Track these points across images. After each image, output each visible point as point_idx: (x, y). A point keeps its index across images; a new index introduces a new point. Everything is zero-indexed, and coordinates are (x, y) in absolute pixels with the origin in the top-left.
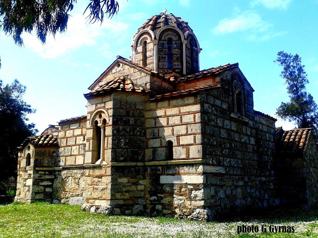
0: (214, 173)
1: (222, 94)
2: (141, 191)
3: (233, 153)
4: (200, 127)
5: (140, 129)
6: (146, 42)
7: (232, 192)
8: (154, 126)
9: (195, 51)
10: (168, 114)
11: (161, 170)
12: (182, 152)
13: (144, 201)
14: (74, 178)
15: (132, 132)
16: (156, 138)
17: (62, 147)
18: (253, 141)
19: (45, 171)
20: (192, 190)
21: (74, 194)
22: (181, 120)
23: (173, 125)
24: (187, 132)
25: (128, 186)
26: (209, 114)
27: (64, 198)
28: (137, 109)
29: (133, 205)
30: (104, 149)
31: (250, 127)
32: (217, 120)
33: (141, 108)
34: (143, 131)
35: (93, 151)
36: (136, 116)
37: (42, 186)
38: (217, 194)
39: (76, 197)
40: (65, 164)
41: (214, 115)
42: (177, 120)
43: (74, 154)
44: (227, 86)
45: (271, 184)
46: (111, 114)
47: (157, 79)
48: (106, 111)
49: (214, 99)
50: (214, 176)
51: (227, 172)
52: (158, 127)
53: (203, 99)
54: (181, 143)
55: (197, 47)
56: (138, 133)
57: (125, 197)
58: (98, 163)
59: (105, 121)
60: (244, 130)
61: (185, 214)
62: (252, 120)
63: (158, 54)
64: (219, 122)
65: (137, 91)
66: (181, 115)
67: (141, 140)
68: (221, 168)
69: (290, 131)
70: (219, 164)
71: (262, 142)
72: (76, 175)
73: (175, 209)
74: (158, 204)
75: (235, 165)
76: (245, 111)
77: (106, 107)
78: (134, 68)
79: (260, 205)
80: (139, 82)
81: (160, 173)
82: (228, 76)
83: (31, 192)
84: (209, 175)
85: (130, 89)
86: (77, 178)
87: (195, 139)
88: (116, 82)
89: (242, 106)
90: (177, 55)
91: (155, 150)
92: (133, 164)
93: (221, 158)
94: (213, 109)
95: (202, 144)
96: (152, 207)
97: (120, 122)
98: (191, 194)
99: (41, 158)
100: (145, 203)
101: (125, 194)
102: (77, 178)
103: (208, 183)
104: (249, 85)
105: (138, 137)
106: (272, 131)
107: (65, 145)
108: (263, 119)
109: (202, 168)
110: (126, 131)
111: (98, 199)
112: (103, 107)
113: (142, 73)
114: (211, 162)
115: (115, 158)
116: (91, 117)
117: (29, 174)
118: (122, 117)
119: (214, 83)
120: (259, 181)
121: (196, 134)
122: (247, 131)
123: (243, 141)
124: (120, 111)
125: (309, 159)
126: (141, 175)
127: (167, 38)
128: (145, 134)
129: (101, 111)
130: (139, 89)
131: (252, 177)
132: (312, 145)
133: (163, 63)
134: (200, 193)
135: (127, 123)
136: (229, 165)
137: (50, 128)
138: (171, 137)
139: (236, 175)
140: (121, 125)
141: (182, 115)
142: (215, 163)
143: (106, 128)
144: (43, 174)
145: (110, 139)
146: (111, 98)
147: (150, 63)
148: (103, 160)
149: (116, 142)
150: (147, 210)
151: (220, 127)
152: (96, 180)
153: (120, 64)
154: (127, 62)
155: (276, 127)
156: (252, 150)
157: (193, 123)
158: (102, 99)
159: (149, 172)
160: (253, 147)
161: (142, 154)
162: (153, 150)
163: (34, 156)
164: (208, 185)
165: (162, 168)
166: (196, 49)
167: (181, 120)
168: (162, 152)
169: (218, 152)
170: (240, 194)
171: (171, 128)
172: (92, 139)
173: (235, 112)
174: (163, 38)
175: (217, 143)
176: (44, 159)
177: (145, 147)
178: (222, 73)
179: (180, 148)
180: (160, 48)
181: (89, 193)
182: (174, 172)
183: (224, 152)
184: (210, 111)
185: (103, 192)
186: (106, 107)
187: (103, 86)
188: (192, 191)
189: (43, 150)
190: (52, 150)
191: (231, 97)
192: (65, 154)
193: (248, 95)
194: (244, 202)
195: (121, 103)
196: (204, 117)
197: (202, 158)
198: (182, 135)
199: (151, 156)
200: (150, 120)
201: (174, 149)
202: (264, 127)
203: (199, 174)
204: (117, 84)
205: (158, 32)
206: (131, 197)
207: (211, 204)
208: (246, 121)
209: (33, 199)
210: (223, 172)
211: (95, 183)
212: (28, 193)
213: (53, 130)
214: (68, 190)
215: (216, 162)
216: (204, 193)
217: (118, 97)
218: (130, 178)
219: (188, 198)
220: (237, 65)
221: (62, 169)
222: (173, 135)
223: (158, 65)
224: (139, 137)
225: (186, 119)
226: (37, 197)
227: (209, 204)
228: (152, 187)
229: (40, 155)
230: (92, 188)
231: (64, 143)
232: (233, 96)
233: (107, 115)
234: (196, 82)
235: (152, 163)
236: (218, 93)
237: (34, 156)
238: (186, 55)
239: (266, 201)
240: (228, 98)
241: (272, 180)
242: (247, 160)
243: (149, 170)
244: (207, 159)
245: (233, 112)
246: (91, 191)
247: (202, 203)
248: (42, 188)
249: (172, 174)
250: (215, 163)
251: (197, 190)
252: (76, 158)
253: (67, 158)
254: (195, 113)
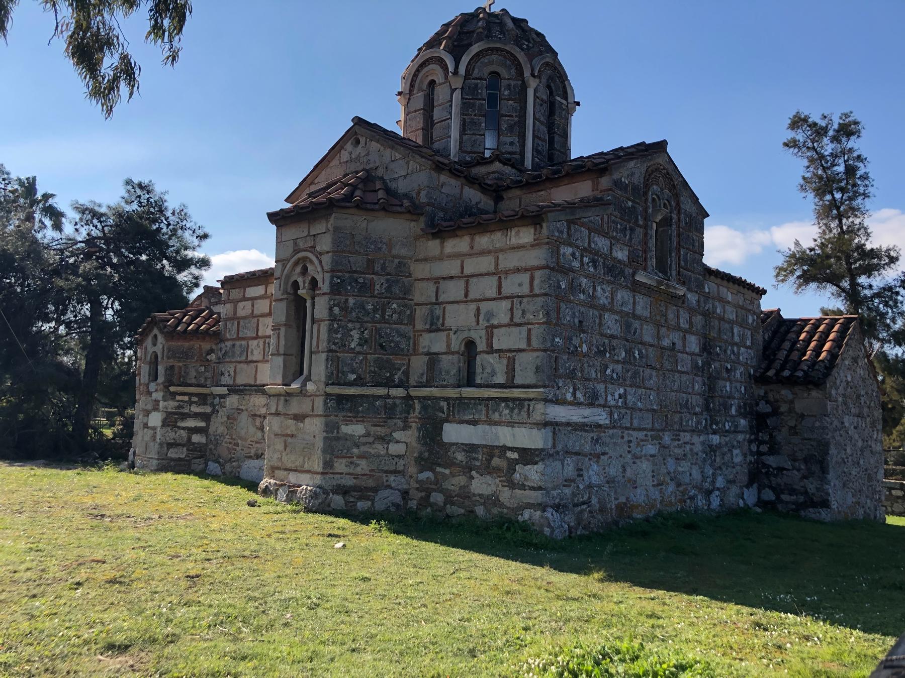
0: (576, 424)
1: (614, 222)
2: (396, 456)
3: (636, 374)
7: (624, 470)
8: (434, 301)
11: (445, 408)
12: (497, 370)
13: (403, 480)
15: (380, 312)
16: (438, 330)
18: (693, 343)
19: (191, 395)
25: (365, 444)
28: (394, 257)
29: (375, 490)
30: (311, 353)
32: (594, 290)
33: (403, 252)
34: (408, 312)
35: (287, 355)
36: (389, 274)
37: (184, 428)
42: (487, 287)
43: (254, 359)
45: (735, 452)
47: (449, 179)
48: (317, 257)
50: (575, 430)
51: (615, 422)
52: (442, 303)
53: (557, 234)
56: (395, 316)
57: (359, 470)
59: (314, 283)
60: (671, 316)
63: (462, 114)
64: (603, 295)
66: (499, 274)
70: (592, 401)
71: (720, 347)
74: (434, 490)
75: (639, 404)
77: (318, 248)
81: (443, 416)
82: (637, 176)
86: (260, 416)
89: (670, 254)
90: (511, 116)
91: (433, 358)
93: (601, 387)
96: (422, 497)
97: (349, 288)
99: (181, 364)
100: (405, 487)
101: (358, 462)
103: (559, 447)
106: (750, 321)
110: (364, 308)
112: (310, 247)
114: (569, 397)
118: (355, 275)
119: (596, 193)
120: (703, 443)
123: (666, 344)
127: (486, 71)
128: (411, 320)
129: (307, 257)
133: (474, 138)
135: (365, 289)
136: (620, 404)
140: (353, 295)
142: (582, 400)
144: (186, 402)
145: (324, 327)
148: (308, 378)
149: (339, 336)
150: (409, 502)
151: (603, 308)
156: (689, 366)
159: (417, 411)
160: (692, 360)
161: (402, 369)
162: (429, 358)
164: (558, 453)
165: (448, 404)
166: (564, 102)
172: (285, 325)
175: (589, 348)
176: (187, 368)
177: (411, 351)
179: (491, 359)
180: (466, 99)
182: (477, 417)
183: (608, 371)
184: (576, 264)
191: (639, 231)
194: (655, 494)
195: (353, 238)
196: (558, 282)
198: (499, 326)
199: (422, 374)
200: (424, 284)
207: (561, 499)
208: (678, 292)
209: (163, 459)
210: (601, 422)
218: (372, 425)
220: (661, 146)
223: (461, 143)
225: (511, 286)
228: (424, 449)
229: (179, 357)
233: (319, 269)
234: (550, 189)
235: (425, 392)
236: (602, 219)
238: (535, 118)
241: (739, 442)
242: (672, 391)
243: (418, 407)
248: (183, 433)
249: (473, 421)
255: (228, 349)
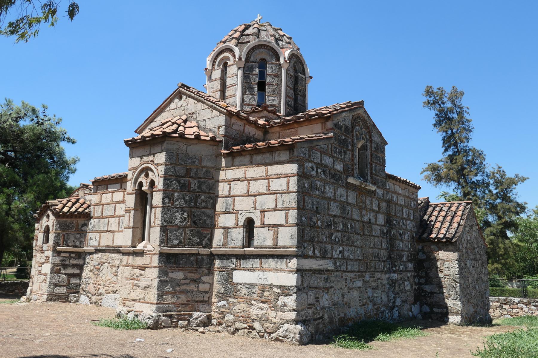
0: (315, 270)
3: (349, 238)
4: (296, 199)
5: (206, 198)
6: (227, 63)
9: (301, 80)
10: (249, 176)
14: (110, 266)
17: (95, 219)
18: (381, 219)
20: (279, 295)
21: (110, 289)
22: (268, 186)
23: (255, 193)
24: (276, 205)
25: (183, 285)
26: (311, 179)
27: (96, 294)
30: (150, 227)
31: (379, 199)
32: (325, 188)
33: (209, 164)
34: (211, 201)
36: (200, 178)
38: (318, 301)
39: (112, 294)
40: (99, 244)
41: (321, 180)
44: (344, 135)
46: (162, 173)
47: (237, 121)
49: (321, 155)
53: (302, 155)
54: (266, 223)
55: (304, 74)
58: (140, 247)
60: (368, 203)
61: (267, 330)
62: (382, 188)
64: (329, 191)
65: (202, 138)
67: (208, 214)
68: (326, 261)
69: (440, 204)
70: (324, 255)
72: (113, 261)
73: (253, 322)
76: (372, 173)
77: (156, 162)
78: (203, 102)
79: (387, 315)
80: (209, 125)
82: (347, 121)
83: (48, 282)
84: (306, 272)
85: (193, 135)
86: (115, 266)
87: (287, 216)
88: (174, 123)
89: (367, 166)
92: (194, 250)
93: (329, 247)
94: (319, 170)
95: (297, 225)
98: (277, 302)
101: (179, 296)
102: (115, 266)
103: (305, 286)
104: (380, 135)
105: (203, 210)
106: (412, 205)
107: (100, 215)
108: (398, 187)
109: (296, 262)
111: (139, 301)
113: (214, 111)
114: (311, 253)
115: (164, 242)
116: (133, 175)
117: (47, 257)
121: (289, 210)
122: (372, 204)
124: (176, 168)
125: (466, 248)
126: (205, 268)
130: (208, 136)
131: (376, 274)
132: (471, 227)
134: (291, 301)
136: (340, 257)
137: (82, 189)
138: (252, 211)
139: (351, 272)
141: (270, 179)
142: (318, 255)
143: (154, 193)
145: (159, 211)
146: (163, 148)
147: (231, 96)
151: (330, 199)
152: (137, 272)
153: (183, 96)
154: (193, 93)
155: (419, 198)
156: (379, 232)
157: (286, 193)
158: (150, 149)
163: (54, 229)
164: (304, 288)
166: (303, 76)
167: (268, 186)
168: (238, 235)
169: (324, 238)
170: (356, 300)
171: (253, 198)
172: (134, 210)
173: (356, 175)
174: (252, 59)
175: (322, 224)
176: (69, 235)
178: (335, 115)
180: (246, 73)
181: (127, 291)
183: (333, 237)
184: (314, 173)
185: (146, 291)
186: (156, 162)
187: (154, 129)
188: (279, 297)
189: (68, 220)
190: (81, 221)
191: (349, 153)
192: (100, 230)
193: (378, 149)
196: (304, 183)
197: (297, 248)
198: (268, 210)
201: (256, 230)
202: (400, 198)
203: (291, 272)
204: (175, 126)
205: (246, 49)
206: (188, 301)
207: (307, 317)
210: (329, 268)
211: (134, 277)
212: (44, 284)
213: (86, 192)
214: (102, 283)
215: (320, 252)
216: (297, 300)
217: (175, 147)
219: (273, 307)
221: (95, 251)
222: (255, 210)
224: (205, 210)
226: (58, 290)
227: (304, 317)
230: (131, 285)
231: (99, 213)
232: (353, 151)
233: (157, 174)
234: (297, 128)
237: (54, 229)
239: (397, 309)
240: (345, 153)
241: (408, 277)
242: (369, 248)
244: (305, 248)
245: (353, 176)
246: (129, 288)
247: (293, 315)
250: (318, 255)
251: (287, 296)
252: (114, 236)
253: (102, 234)
254: (290, 177)
255: (95, 223)
